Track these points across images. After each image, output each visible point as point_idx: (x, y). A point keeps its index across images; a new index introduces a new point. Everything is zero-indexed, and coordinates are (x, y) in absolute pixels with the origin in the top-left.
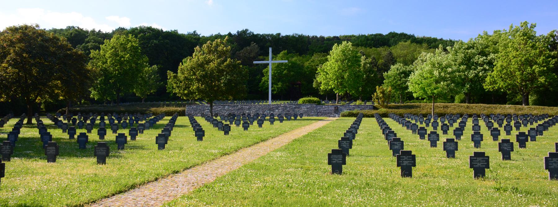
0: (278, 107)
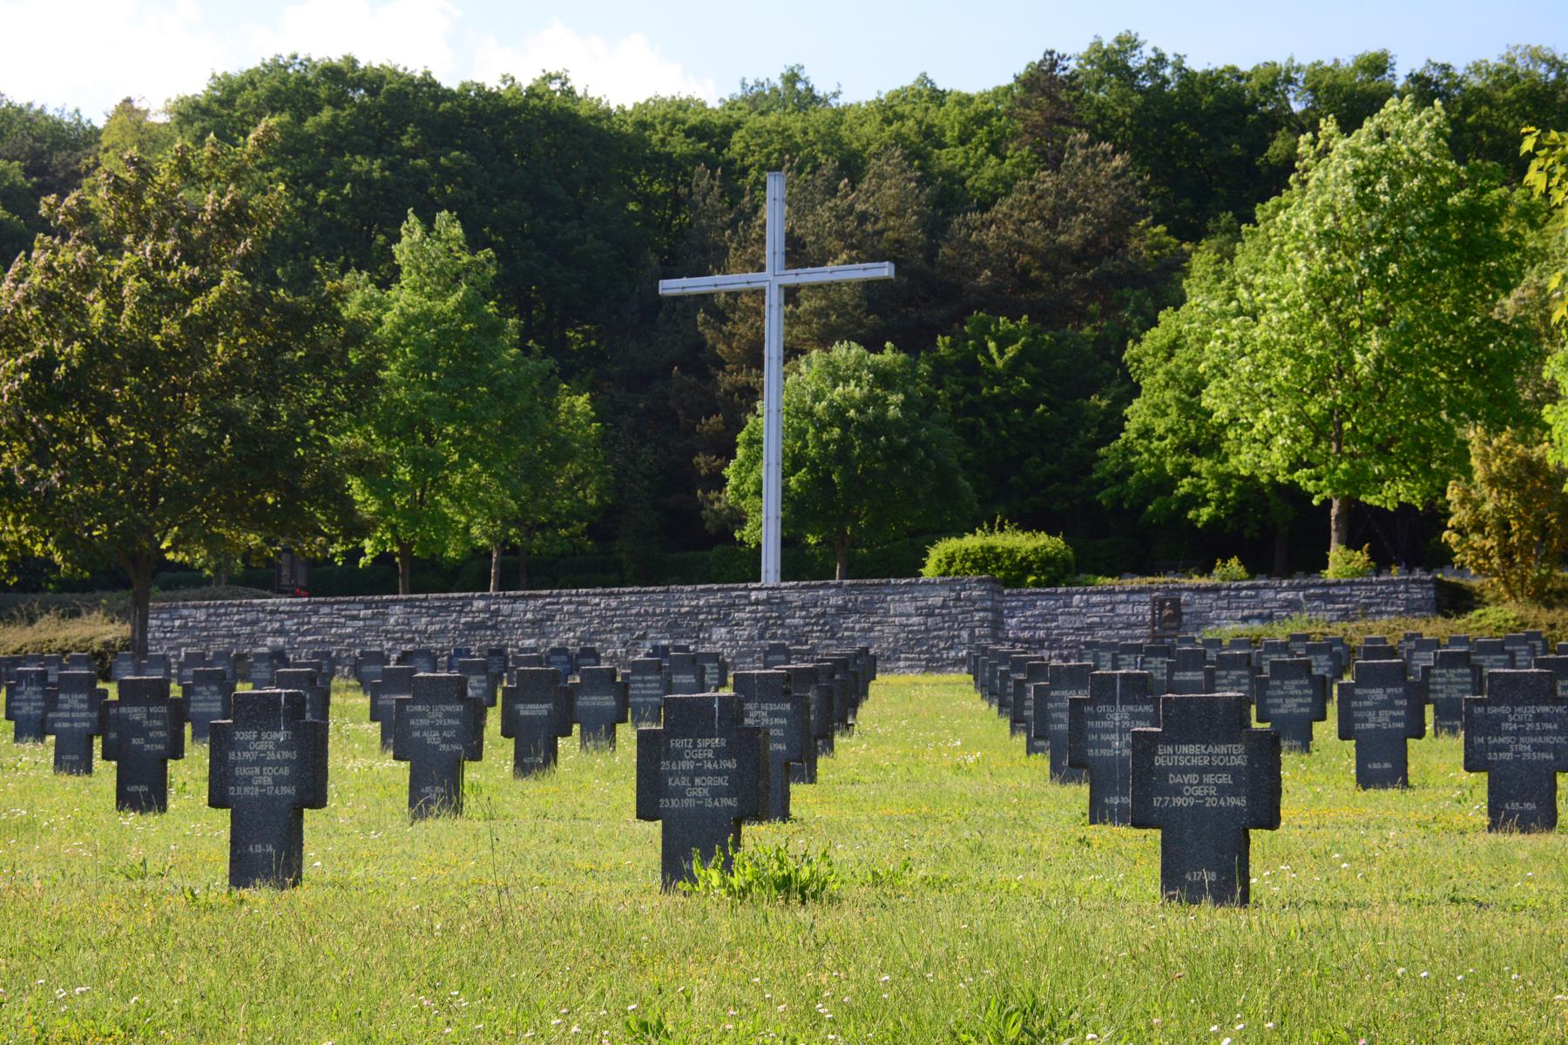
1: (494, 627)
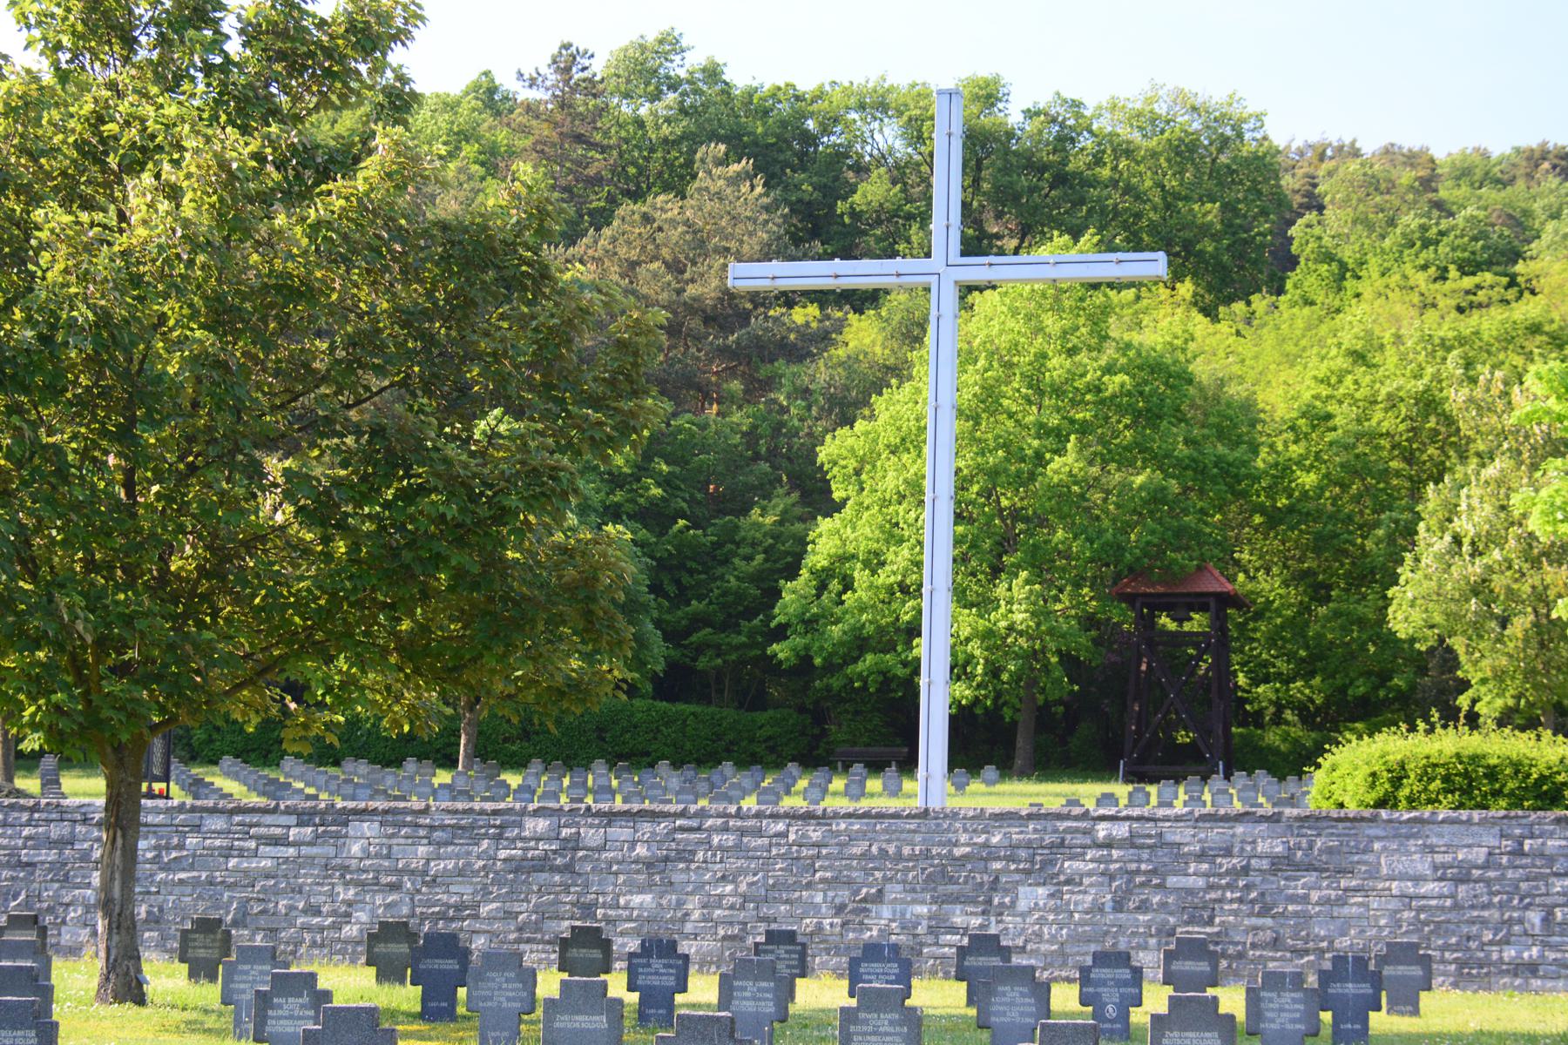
0: (1044, 856)
1: (568, 869)
